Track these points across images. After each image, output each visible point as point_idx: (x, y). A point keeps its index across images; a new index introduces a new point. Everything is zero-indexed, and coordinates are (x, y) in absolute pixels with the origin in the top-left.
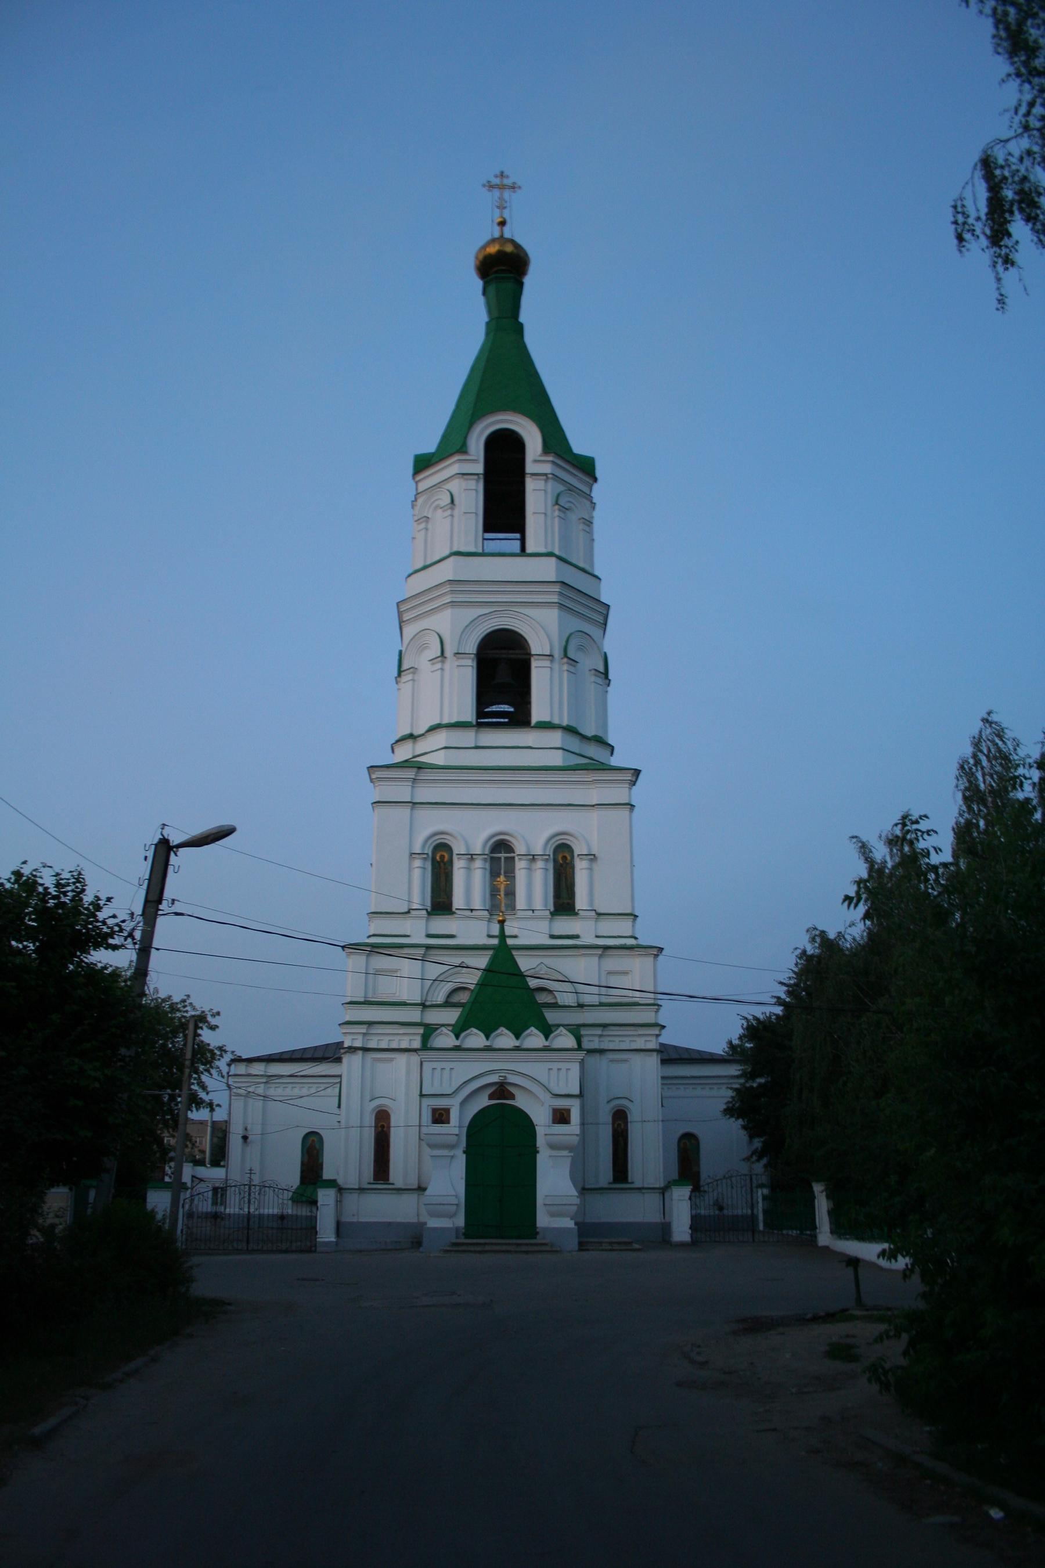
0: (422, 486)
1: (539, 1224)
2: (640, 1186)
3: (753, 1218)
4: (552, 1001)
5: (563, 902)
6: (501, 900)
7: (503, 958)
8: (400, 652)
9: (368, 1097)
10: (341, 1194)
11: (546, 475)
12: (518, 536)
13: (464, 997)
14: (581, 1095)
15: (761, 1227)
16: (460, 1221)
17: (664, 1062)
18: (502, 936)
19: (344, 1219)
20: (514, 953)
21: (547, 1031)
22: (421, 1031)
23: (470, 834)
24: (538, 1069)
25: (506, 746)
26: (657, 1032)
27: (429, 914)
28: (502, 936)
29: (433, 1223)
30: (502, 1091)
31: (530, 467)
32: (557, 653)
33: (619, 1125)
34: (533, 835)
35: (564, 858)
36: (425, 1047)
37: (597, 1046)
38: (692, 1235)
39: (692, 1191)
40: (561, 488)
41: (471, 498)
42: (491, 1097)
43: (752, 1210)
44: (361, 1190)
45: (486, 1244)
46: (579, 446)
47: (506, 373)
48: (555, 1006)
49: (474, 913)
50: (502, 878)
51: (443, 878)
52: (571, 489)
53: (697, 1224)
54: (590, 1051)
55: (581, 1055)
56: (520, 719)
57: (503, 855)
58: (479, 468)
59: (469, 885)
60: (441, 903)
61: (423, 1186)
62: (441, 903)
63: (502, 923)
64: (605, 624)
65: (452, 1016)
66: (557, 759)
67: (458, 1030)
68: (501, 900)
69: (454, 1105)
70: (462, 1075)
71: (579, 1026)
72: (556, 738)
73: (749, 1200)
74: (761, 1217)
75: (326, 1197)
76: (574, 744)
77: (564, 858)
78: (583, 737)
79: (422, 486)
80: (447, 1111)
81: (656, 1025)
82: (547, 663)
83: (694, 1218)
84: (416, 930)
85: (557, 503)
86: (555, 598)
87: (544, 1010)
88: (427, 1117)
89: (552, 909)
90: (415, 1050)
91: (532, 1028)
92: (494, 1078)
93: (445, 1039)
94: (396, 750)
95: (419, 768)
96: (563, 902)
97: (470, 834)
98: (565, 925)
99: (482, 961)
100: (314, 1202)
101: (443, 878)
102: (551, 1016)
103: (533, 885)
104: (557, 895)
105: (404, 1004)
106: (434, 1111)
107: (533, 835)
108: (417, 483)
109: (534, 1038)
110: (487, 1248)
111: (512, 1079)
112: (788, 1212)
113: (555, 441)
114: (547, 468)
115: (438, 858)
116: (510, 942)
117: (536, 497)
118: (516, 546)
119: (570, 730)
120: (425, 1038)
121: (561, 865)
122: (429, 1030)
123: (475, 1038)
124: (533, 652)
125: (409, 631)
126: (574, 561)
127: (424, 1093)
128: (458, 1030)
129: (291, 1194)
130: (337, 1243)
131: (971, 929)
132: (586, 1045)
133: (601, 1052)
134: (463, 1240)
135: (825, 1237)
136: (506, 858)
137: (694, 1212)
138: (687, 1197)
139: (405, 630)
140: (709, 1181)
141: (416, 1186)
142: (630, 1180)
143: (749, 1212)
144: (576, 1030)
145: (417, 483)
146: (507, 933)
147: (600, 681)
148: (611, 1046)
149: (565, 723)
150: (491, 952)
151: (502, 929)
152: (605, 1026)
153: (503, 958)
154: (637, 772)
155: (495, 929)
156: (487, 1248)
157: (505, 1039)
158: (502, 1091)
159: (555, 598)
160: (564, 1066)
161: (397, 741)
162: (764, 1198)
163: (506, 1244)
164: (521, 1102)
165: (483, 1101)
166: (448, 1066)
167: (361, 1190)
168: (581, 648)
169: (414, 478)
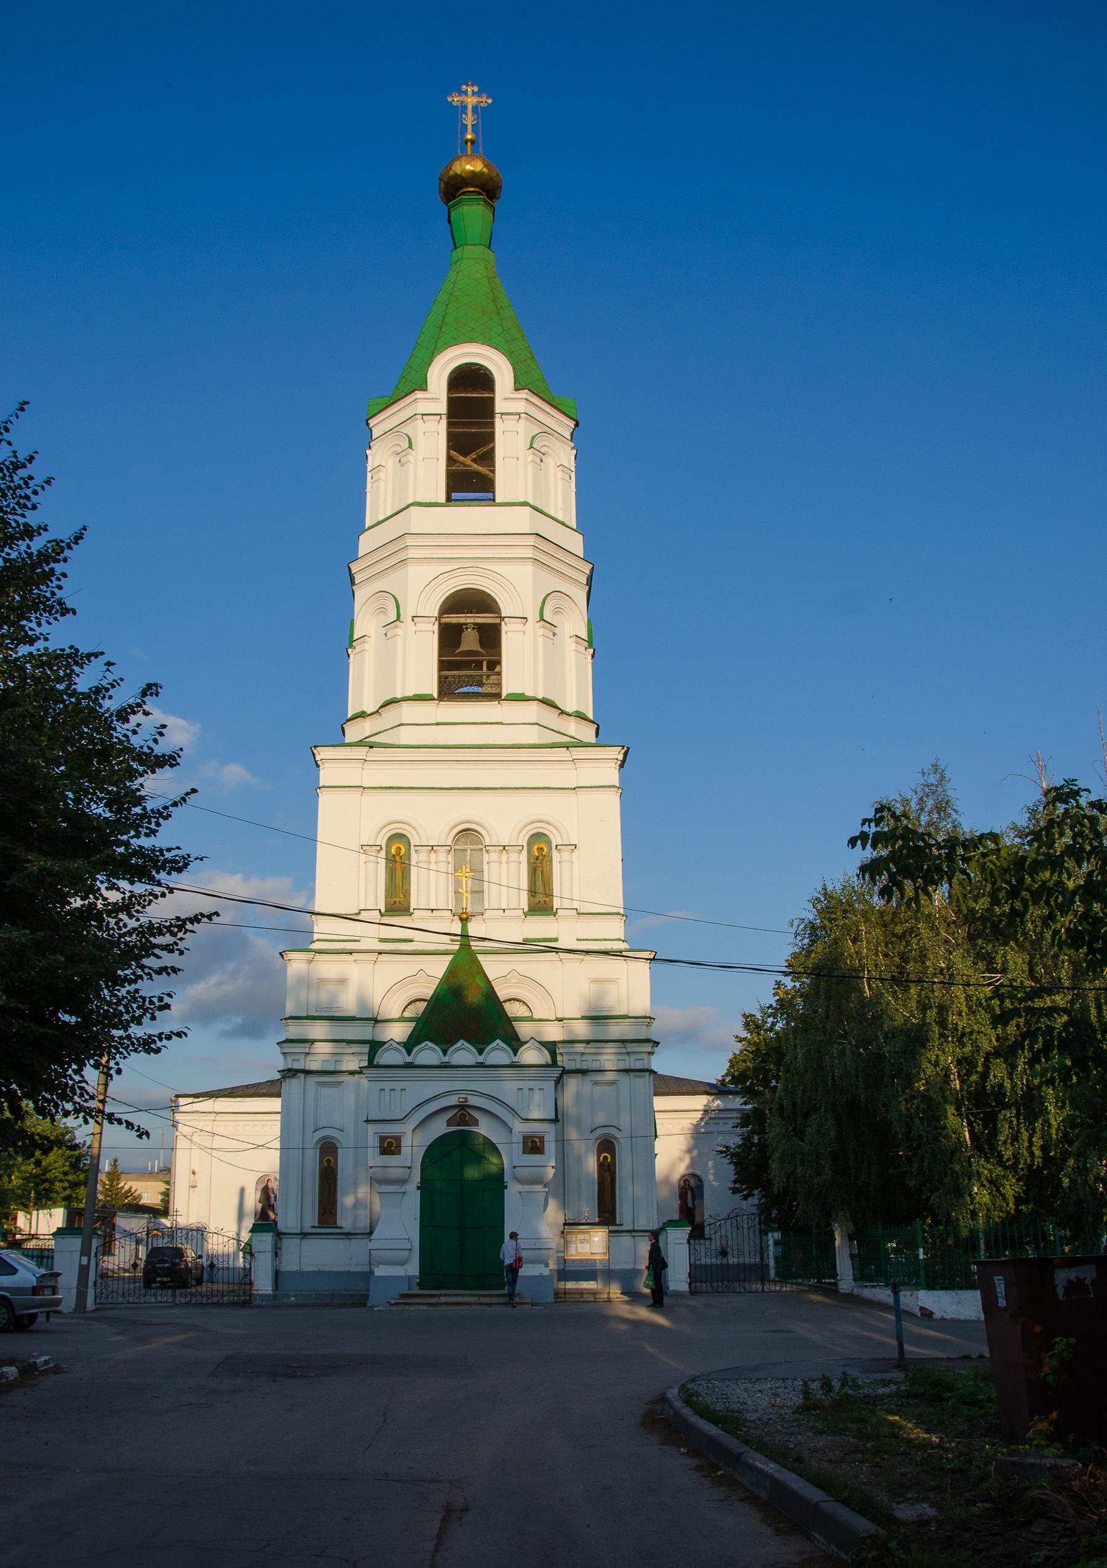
3: (764, 1267)
4: (528, 1014)
5: (541, 902)
7: (465, 958)
9: (310, 1127)
10: (281, 1239)
11: (519, 414)
14: (555, 1120)
15: (772, 1273)
16: (413, 1269)
19: (285, 1268)
26: (649, 1049)
29: (380, 1271)
30: (463, 1114)
31: (500, 406)
33: (605, 1157)
34: (505, 822)
35: (540, 849)
36: (371, 1064)
37: (579, 1067)
39: (692, 1236)
42: (449, 1123)
43: (762, 1258)
44: (304, 1235)
45: (441, 1295)
49: (435, 913)
51: (399, 873)
52: (548, 431)
53: (696, 1273)
58: (442, 407)
59: (431, 885)
60: (397, 905)
62: (397, 905)
66: (532, 735)
67: (409, 1045)
69: (406, 1130)
72: (531, 711)
73: (758, 1242)
74: (772, 1262)
76: (550, 717)
77: (540, 849)
80: (398, 1139)
81: (648, 1041)
82: (520, 627)
85: (531, 447)
86: (529, 553)
88: (373, 1141)
89: (526, 910)
91: (498, 1041)
92: (453, 1100)
95: (371, 747)
96: (541, 902)
97: (431, 821)
98: (539, 928)
101: (399, 873)
103: (508, 880)
104: (532, 893)
106: (382, 1139)
107: (505, 822)
109: (498, 1053)
110: (443, 1299)
111: (473, 1101)
112: (807, 1261)
114: (520, 407)
115: (393, 851)
119: (546, 702)
121: (537, 858)
123: (429, 1054)
126: (552, 514)
130: (274, 1297)
131: (1075, 1079)
134: (416, 1291)
135: (846, 1281)
138: (685, 1241)
140: (712, 1221)
142: (618, 1222)
143: (758, 1260)
149: (540, 697)
150: (450, 957)
151: (464, 928)
153: (465, 958)
156: (443, 1299)
157: (463, 1053)
158: (463, 1114)
159: (529, 553)
162: (776, 1243)
163: (468, 1295)
164: (484, 1128)
165: (440, 1127)
166: (398, 1086)
167: (304, 1235)
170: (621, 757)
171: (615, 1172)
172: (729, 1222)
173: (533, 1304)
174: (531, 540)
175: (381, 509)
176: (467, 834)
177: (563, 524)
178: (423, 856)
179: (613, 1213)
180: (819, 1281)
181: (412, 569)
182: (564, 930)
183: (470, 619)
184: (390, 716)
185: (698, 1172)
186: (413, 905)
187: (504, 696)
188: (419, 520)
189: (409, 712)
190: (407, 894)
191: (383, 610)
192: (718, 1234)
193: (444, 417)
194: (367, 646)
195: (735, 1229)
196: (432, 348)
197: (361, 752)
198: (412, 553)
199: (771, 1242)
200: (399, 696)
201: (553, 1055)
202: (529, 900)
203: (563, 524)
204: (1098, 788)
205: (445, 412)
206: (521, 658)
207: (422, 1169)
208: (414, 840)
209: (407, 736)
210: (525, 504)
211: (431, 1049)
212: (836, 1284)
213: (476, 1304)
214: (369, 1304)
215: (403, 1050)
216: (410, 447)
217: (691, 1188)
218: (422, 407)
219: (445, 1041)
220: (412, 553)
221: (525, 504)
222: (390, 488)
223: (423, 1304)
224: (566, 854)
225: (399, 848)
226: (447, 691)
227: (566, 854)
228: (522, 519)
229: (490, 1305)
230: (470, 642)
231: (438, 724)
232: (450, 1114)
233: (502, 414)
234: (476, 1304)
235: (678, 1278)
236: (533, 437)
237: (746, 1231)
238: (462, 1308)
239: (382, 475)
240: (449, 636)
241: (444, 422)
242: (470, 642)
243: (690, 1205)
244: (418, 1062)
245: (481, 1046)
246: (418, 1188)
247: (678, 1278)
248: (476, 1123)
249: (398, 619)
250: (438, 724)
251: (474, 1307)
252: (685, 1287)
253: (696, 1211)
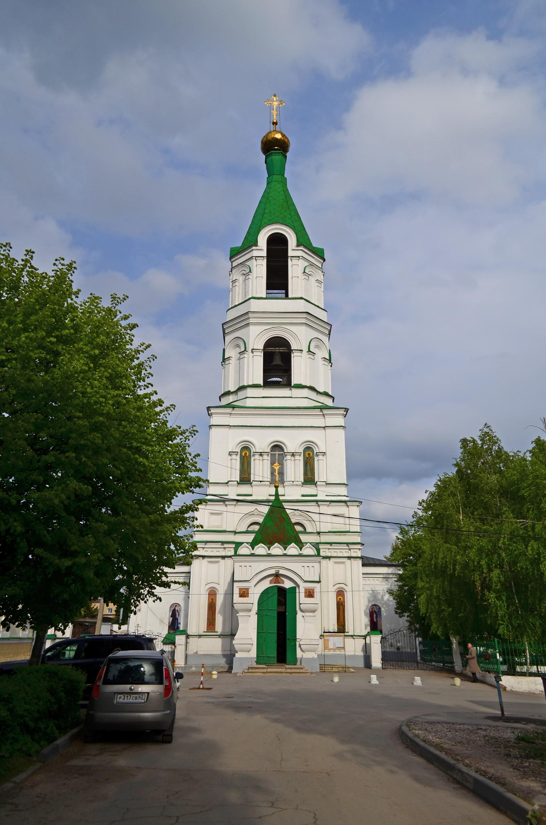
0: (235, 264)
1: (297, 656)
2: (353, 634)
5: (309, 479)
6: (278, 478)
7: (277, 507)
8: (224, 350)
11: (299, 257)
12: (284, 291)
13: (256, 528)
16: (253, 654)
17: (364, 565)
18: (277, 495)
20: (283, 504)
21: (301, 545)
22: (234, 546)
23: (261, 441)
24: (296, 566)
25: (278, 396)
27: (238, 484)
28: (277, 495)
31: (290, 253)
32: (305, 349)
33: (340, 599)
34: (293, 442)
38: (382, 664)
40: (307, 264)
41: (260, 269)
44: (200, 636)
46: (315, 244)
47: (277, 204)
48: (305, 532)
50: (277, 464)
51: (246, 465)
52: (312, 264)
53: (386, 657)
54: (324, 558)
55: (318, 559)
56: (288, 384)
57: (277, 453)
58: (264, 254)
59: (261, 469)
60: (245, 479)
61: (234, 633)
62: (245, 479)
63: (277, 487)
64: (329, 334)
65: (250, 538)
67: (253, 545)
68: (278, 478)
70: (255, 573)
71: (318, 544)
72: (306, 392)
75: (180, 639)
76: (313, 395)
78: (318, 392)
79: (235, 264)
82: (299, 354)
83: (384, 653)
84: (232, 492)
85: (304, 272)
87: (300, 535)
89: (303, 481)
90: (230, 557)
91: (293, 544)
92: (273, 572)
93: (244, 550)
94: (222, 399)
96: (309, 479)
97: (261, 441)
99: (265, 509)
100: (174, 643)
102: (303, 538)
103: (294, 469)
104: (305, 474)
105: (225, 531)
106: (240, 589)
108: (232, 262)
109: (293, 549)
111: (282, 572)
113: (304, 242)
114: (300, 253)
116: (281, 498)
117: (295, 269)
118: (284, 295)
120: (236, 550)
121: (308, 458)
122: (238, 545)
123: (261, 549)
124: (292, 349)
125: (228, 338)
127: (235, 580)
128: (253, 545)
129: (163, 639)
132: (322, 554)
133: (329, 558)
134: (255, 665)
136: (278, 454)
137: (383, 650)
138: (379, 642)
139: (226, 338)
141: (230, 634)
144: (316, 546)
145: (232, 262)
146: (280, 494)
147: (327, 363)
148: (334, 554)
149: (308, 385)
152: (331, 544)
153: (277, 507)
154: (347, 410)
155: (272, 491)
157: (277, 549)
160: (311, 565)
161: (222, 395)
165: (266, 584)
167: (200, 636)
168: (317, 347)
169: (230, 260)
170: (345, 413)
171: (344, 606)
172: (400, 633)
173: (311, 673)
174: (305, 315)
175: (237, 299)
176: (277, 447)
177: (318, 307)
178: (257, 457)
179: (344, 626)
180: (444, 665)
181: (251, 327)
182: (322, 493)
183: (277, 350)
184: (241, 394)
185: (373, 603)
186: (252, 479)
187: (292, 384)
188: (254, 306)
189: (250, 392)
190: (249, 474)
191: (238, 346)
192: (395, 639)
193: (265, 258)
194: (230, 361)
195: (403, 637)
196: (259, 225)
197: (229, 410)
198: (251, 320)
199: (417, 642)
200: (246, 384)
201: (318, 550)
202: (304, 477)
203: (318, 307)
204: (517, 443)
205: (266, 255)
206: (301, 368)
207: (258, 605)
208: (253, 450)
209: (249, 403)
210: (301, 298)
211: (263, 547)
212: (453, 667)
213: (285, 672)
214: (233, 672)
215: (250, 547)
216: (250, 272)
217: (375, 612)
218: (255, 253)
219: (269, 544)
220: (251, 320)
221: (301, 298)
222: (241, 289)
223: (260, 672)
224: (321, 457)
225: (246, 453)
226: (267, 384)
227: (321, 457)
228: (301, 306)
229: (291, 673)
230: (277, 361)
231: (263, 397)
232: (271, 578)
233: (292, 257)
234: (285, 672)
235: (377, 661)
236: (305, 267)
237: (408, 638)
238: (277, 674)
239: (237, 284)
240: (268, 357)
241: (265, 260)
242: (277, 361)
243: (375, 620)
244: (257, 553)
245: (285, 546)
246: (256, 613)
247: (377, 661)
248: (283, 582)
249: (245, 350)
250: (263, 397)
251: (284, 674)
252: (380, 665)
253: (378, 624)
